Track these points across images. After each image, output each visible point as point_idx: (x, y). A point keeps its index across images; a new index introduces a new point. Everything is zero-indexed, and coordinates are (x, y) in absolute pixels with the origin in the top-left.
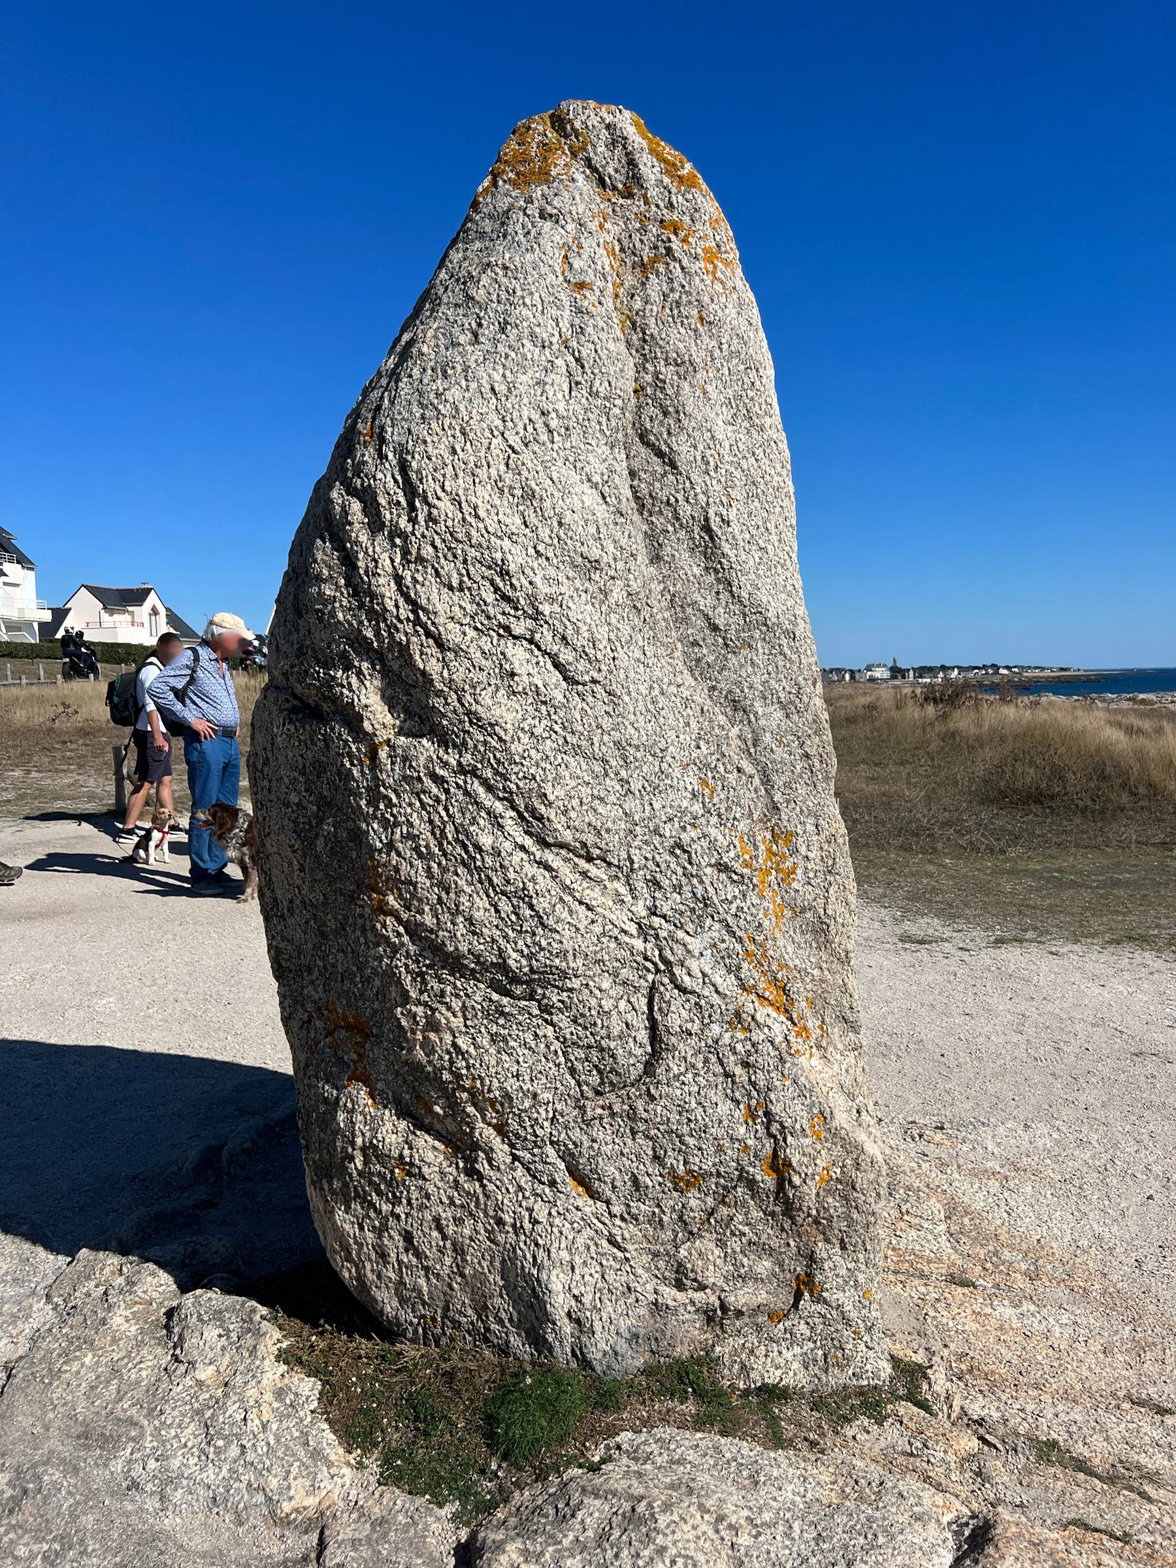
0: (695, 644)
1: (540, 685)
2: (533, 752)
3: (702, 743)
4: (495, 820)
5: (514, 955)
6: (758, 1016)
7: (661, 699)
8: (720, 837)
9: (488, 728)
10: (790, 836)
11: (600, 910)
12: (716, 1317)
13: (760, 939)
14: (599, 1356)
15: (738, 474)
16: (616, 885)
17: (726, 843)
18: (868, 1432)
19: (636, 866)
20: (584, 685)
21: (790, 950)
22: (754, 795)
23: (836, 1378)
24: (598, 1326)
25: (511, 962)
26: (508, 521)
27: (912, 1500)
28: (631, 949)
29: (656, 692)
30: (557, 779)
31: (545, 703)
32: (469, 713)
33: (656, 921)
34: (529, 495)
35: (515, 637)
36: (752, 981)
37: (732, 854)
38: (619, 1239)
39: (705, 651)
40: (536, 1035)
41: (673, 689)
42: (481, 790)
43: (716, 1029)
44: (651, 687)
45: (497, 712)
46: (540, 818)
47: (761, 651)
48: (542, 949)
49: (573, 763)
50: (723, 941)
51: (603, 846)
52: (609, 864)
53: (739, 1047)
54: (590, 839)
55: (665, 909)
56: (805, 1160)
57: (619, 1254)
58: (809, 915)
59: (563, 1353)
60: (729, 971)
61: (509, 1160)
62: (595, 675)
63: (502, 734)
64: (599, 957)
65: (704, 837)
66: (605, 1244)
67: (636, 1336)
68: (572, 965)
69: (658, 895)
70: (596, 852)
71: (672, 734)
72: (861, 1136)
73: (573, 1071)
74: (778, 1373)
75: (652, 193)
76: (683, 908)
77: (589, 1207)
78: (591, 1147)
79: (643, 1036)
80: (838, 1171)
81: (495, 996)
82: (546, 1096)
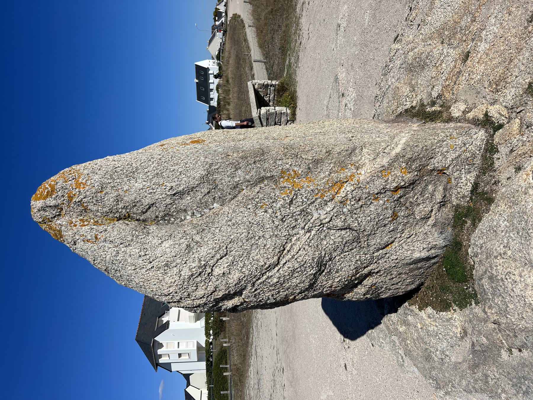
0: (214, 199)
1: (227, 265)
3: (248, 207)
5: (312, 271)
6: (343, 196)
7: (233, 221)
8: (281, 203)
9: (240, 280)
10: (283, 172)
11: (301, 246)
12: (443, 204)
13: (316, 191)
14: (444, 243)
15: (154, 180)
16: (293, 240)
17: (283, 201)
18: (499, 159)
21: (322, 176)
22: (267, 187)
23: (478, 161)
26: (175, 272)
27: (520, 189)
29: (230, 223)
30: (258, 260)
31: (233, 263)
33: (306, 227)
34: (166, 265)
35: (212, 271)
37: (287, 199)
39: (217, 195)
41: (230, 215)
42: (260, 281)
43: (345, 210)
44: (229, 225)
46: (270, 266)
51: (280, 246)
52: (286, 243)
53: (352, 203)
54: (277, 250)
55: (303, 225)
56: (396, 180)
57: (413, 236)
59: (439, 252)
60: (326, 204)
61: (376, 264)
62: (224, 248)
65: (280, 209)
66: (409, 240)
69: (298, 227)
71: (245, 219)
72: (393, 153)
73: (351, 250)
74: (469, 184)
75: (59, 202)
76: (303, 219)
77: (396, 244)
79: (343, 232)
80: (404, 164)
81: (324, 273)
82: (358, 258)
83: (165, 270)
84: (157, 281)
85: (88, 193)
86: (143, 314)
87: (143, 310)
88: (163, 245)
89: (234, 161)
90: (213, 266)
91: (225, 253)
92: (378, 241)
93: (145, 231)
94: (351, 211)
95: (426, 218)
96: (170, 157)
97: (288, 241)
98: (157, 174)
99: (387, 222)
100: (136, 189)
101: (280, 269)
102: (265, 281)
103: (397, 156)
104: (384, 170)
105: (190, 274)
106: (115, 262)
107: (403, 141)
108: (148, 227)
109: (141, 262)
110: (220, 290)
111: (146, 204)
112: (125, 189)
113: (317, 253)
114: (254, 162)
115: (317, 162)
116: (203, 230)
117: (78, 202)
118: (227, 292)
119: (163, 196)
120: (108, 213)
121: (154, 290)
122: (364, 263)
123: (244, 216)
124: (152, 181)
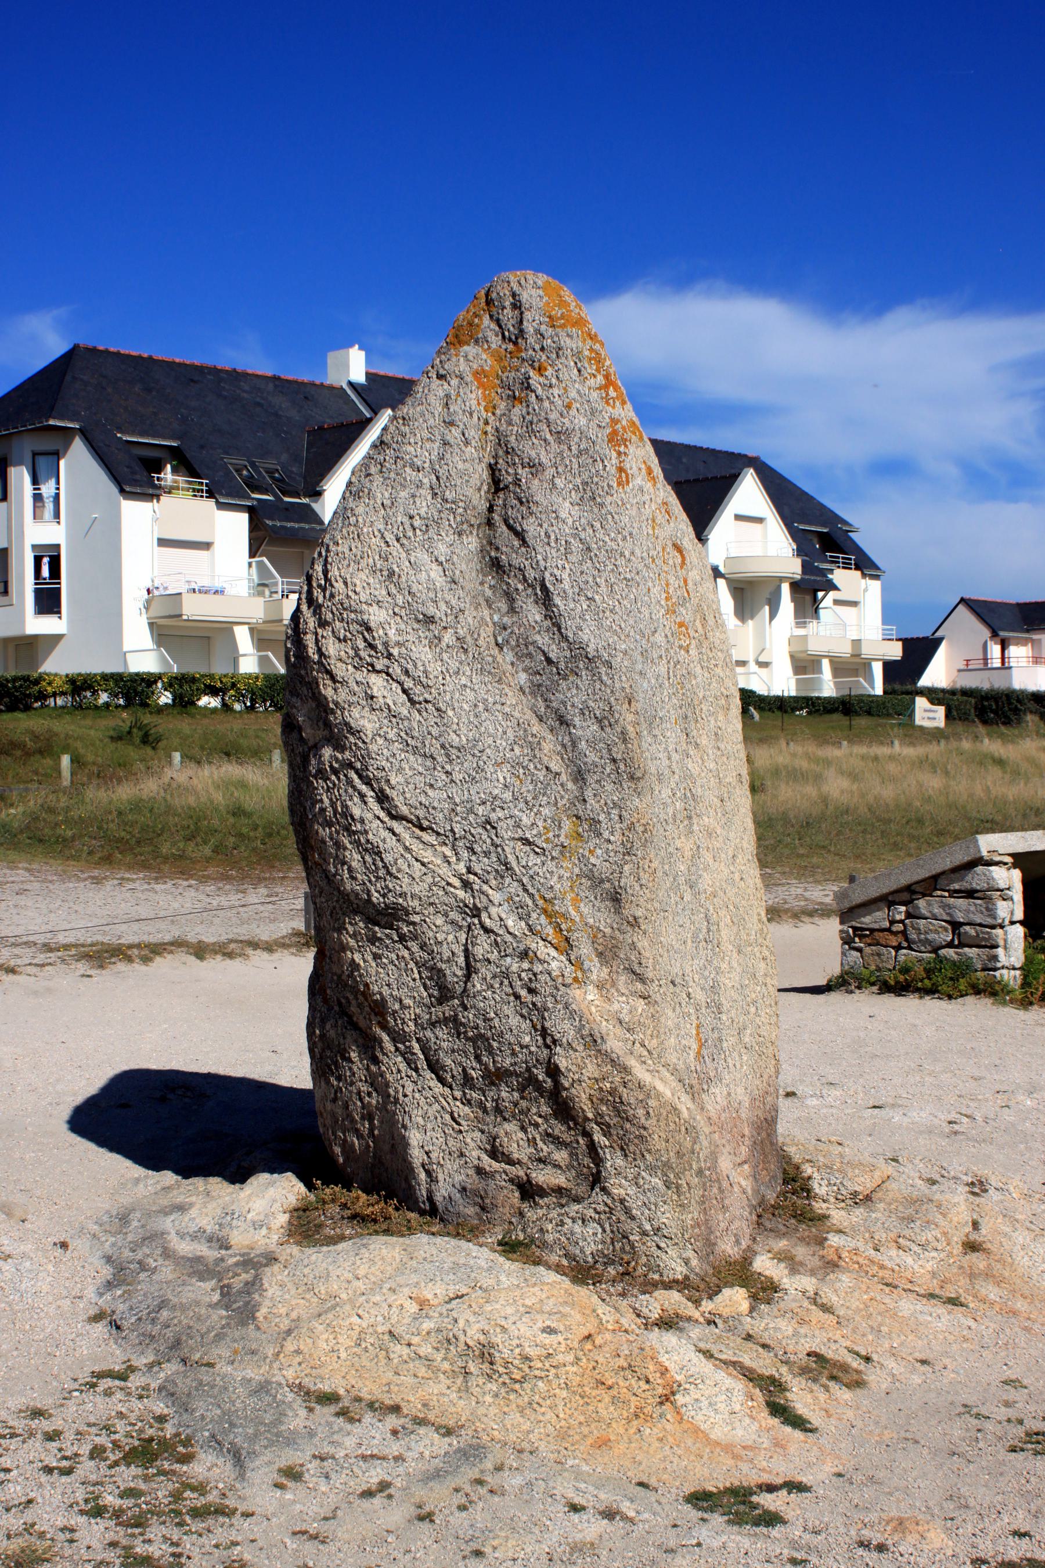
1: (391, 704)
2: (385, 751)
3: (516, 747)
4: (362, 796)
5: (376, 894)
11: (430, 866)
15: (575, 544)
16: (444, 849)
17: (529, 823)
19: (457, 836)
20: (420, 703)
24: (441, 1177)
25: (374, 899)
26: (377, 593)
28: (455, 897)
30: (400, 770)
31: (395, 716)
32: (347, 724)
34: (392, 573)
36: (539, 927)
37: (534, 832)
38: (456, 1115)
40: (398, 955)
44: (475, 705)
45: (362, 722)
47: (584, 677)
48: (390, 891)
49: (412, 758)
50: (518, 896)
51: (431, 819)
53: (523, 975)
54: (421, 813)
55: (477, 868)
58: (607, 885)
63: (364, 737)
64: (432, 900)
65: (511, 817)
66: (448, 1117)
67: (464, 1189)
68: (410, 903)
69: (473, 858)
70: (425, 824)
71: (490, 741)
72: (632, 1062)
75: (531, 340)
76: (489, 869)
77: (438, 1088)
78: (435, 1043)
79: (461, 960)
83: (381, 571)
84: (359, 553)
85: (546, 404)
86: (192, 376)
87: (215, 371)
88: (434, 566)
89: (617, 716)
90: (388, 674)
91: (416, 699)
92: (444, 1045)
93: (465, 526)
94: (506, 974)
95: (495, 1153)
96: (628, 576)
97: (441, 839)
98: (589, 549)
99: (485, 1059)
100: (557, 507)
101: (382, 821)
102: (354, 788)
103: (625, 1070)
104: (593, 1042)
105: (372, 625)
106: (400, 463)
107: (660, 1087)
108: (475, 532)
109: (399, 519)
110: (335, 690)
111: (525, 527)
112: (557, 481)
113: (416, 903)
114: (614, 761)
115: (616, 899)
116: (466, 651)
117: (528, 383)
118: (331, 705)
119: (542, 563)
120: (506, 445)
121: (340, 549)
122: (395, 1020)
123: (497, 735)
124: (575, 539)
